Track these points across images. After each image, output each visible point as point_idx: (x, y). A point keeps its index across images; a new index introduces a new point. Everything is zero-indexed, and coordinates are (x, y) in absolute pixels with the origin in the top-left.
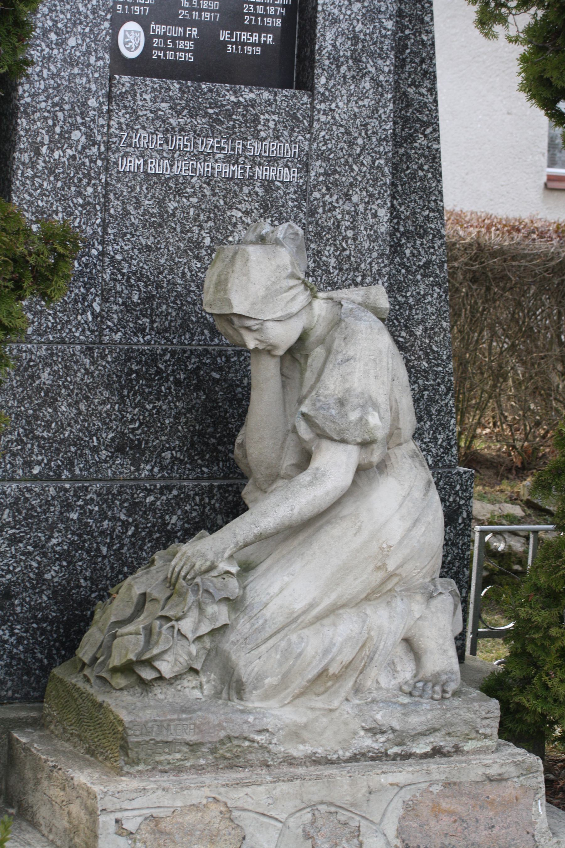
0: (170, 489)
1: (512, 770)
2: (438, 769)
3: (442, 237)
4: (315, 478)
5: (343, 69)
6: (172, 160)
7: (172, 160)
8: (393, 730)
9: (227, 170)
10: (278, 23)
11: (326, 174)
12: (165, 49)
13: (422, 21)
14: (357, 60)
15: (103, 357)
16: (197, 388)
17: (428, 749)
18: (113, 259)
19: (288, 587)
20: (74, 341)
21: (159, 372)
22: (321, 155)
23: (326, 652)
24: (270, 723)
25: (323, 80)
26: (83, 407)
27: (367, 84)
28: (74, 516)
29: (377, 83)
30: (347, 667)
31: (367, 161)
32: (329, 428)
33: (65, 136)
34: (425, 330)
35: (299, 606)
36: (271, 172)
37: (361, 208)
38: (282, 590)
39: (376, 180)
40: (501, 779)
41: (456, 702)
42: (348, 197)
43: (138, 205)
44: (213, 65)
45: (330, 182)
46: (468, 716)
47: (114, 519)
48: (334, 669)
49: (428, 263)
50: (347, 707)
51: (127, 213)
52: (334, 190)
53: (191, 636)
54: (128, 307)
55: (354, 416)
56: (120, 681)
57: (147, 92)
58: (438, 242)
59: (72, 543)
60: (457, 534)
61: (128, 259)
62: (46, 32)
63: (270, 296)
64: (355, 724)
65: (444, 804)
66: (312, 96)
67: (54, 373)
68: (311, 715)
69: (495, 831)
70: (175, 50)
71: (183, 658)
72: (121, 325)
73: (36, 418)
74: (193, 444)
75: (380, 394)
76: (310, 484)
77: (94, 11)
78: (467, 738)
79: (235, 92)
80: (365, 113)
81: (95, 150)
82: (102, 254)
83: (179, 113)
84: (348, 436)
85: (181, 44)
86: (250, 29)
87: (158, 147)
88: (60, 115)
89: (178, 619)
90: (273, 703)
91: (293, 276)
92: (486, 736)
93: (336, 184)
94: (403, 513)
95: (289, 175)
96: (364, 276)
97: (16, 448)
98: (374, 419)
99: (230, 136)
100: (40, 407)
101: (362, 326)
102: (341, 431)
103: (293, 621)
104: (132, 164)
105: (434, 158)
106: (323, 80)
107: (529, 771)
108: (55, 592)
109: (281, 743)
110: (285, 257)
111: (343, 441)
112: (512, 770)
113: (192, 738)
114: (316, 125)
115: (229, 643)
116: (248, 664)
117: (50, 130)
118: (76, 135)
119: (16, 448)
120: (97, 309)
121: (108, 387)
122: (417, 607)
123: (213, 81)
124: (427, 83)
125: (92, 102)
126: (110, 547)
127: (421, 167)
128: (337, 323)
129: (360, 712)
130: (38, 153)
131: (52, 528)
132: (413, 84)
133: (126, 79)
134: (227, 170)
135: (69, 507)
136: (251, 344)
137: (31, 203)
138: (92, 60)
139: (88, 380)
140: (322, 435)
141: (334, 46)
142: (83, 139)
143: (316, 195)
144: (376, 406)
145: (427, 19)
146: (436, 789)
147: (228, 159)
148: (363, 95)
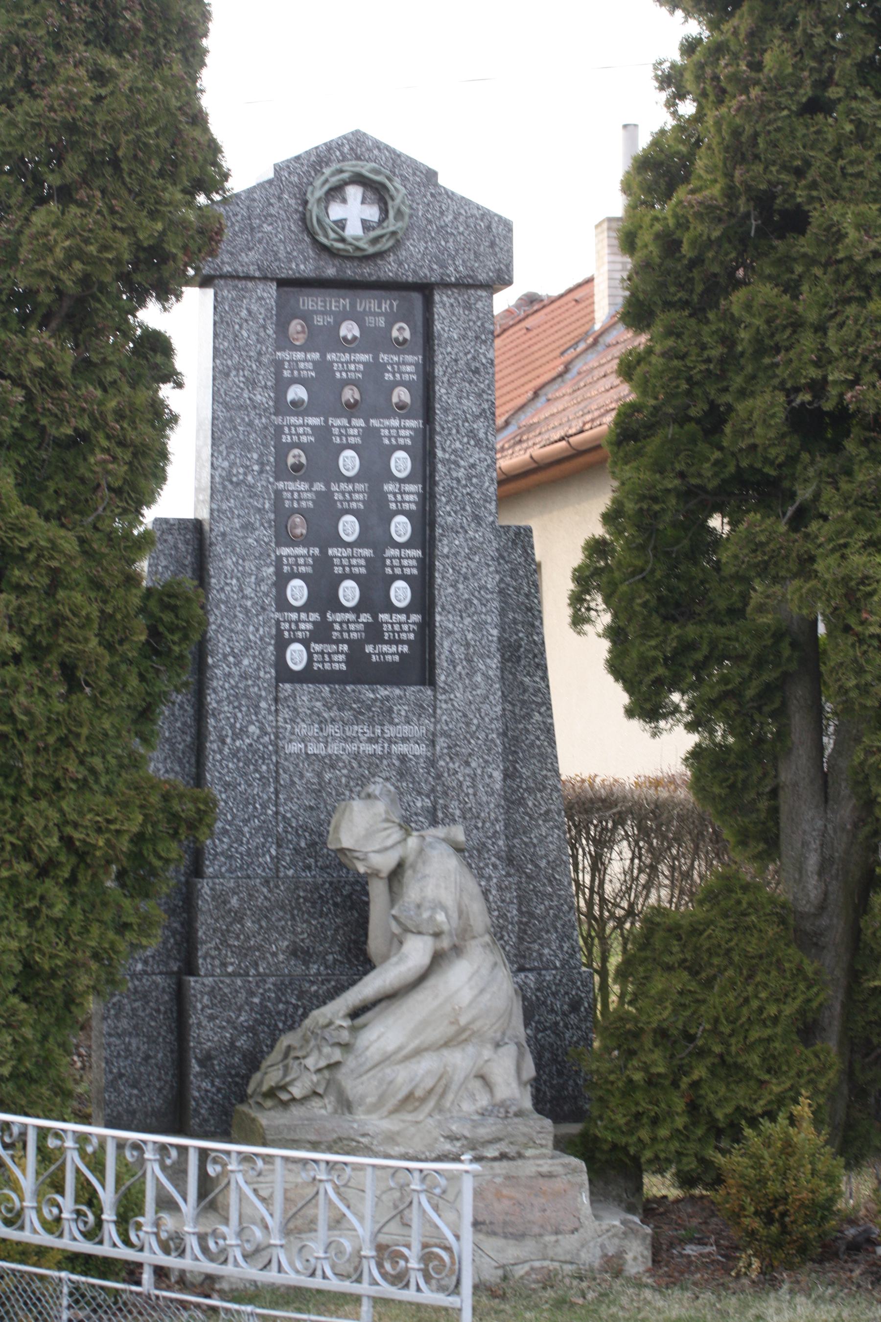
0: (329, 981)
1: (560, 1170)
2: (501, 1167)
3: (558, 790)
4: (401, 960)
5: (459, 668)
6: (326, 744)
7: (326, 744)
8: (466, 1138)
9: (369, 748)
10: (412, 636)
11: (449, 747)
12: (323, 662)
13: (533, 626)
14: (469, 661)
15: (277, 887)
16: (351, 908)
17: (496, 1154)
18: (284, 817)
19: (385, 1034)
20: (257, 876)
21: (321, 897)
22: (444, 734)
23: (412, 1080)
24: (370, 1129)
25: (443, 678)
26: (264, 924)
27: (479, 678)
28: (256, 1000)
29: (486, 677)
30: (430, 1091)
31: (482, 736)
32: (409, 924)
33: (243, 730)
34: (548, 862)
35: (391, 1048)
36: (403, 748)
37: (479, 771)
38: (379, 1038)
39: (489, 750)
40: (550, 1176)
41: (516, 1120)
42: (467, 764)
43: (302, 776)
44: (361, 670)
45: (452, 753)
46: (526, 1130)
47: (287, 1003)
48: (419, 1093)
49: (548, 812)
50: (430, 1121)
51: (293, 783)
52: (456, 759)
53: (312, 1069)
54: (297, 851)
55: (426, 915)
56: (269, 1103)
57: (304, 694)
58: (555, 795)
59: (256, 1020)
60: (580, 1020)
61: (296, 816)
62: (225, 656)
63: (369, 834)
64: (436, 1133)
65: (505, 1192)
66: (434, 691)
67: (241, 900)
68: (402, 1125)
69: (548, 1213)
70: (331, 661)
71: (308, 1084)
72: (293, 864)
73: (228, 931)
74: (349, 950)
75: (449, 899)
76: (397, 963)
77: (262, 639)
78: (526, 1146)
79: (373, 691)
80: (478, 699)
81: (267, 739)
82: (277, 813)
83: (330, 709)
84: (423, 929)
85: (335, 658)
86: (390, 642)
87: (312, 735)
88: (239, 715)
89: (304, 1057)
90: (374, 1117)
91: (387, 820)
92: (542, 1146)
93: (457, 755)
94: (478, 986)
95: (420, 750)
96: (484, 822)
97: (214, 953)
98: (441, 917)
99: (371, 723)
100: (231, 924)
101: (435, 853)
102: (417, 926)
103: (386, 1059)
104: (295, 748)
105: (549, 730)
106: (443, 678)
107: (575, 1171)
108: (244, 1056)
109: (380, 1144)
110: (380, 807)
111: (420, 933)
112: (560, 1170)
113: (313, 1137)
114: (439, 711)
115: (342, 1075)
116: (353, 1087)
117: (232, 726)
118: (252, 729)
119: (214, 953)
120: (274, 853)
121: (282, 908)
122: (487, 1052)
123: (354, 683)
124: (540, 673)
125: (263, 704)
126: (284, 1023)
127: (538, 738)
128: (421, 851)
129: (439, 1124)
130: (224, 742)
131: (240, 1009)
132: (528, 674)
133: (288, 686)
134: (369, 748)
135: (252, 994)
136: (362, 870)
137: (220, 779)
138: (262, 674)
139: (266, 904)
140: (407, 930)
141: (451, 652)
142: (258, 731)
143: (442, 763)
144: (444, 909)
145: (537, 623)
146: (498, 1180)
147: (370, 740)
148: (476, 687)
